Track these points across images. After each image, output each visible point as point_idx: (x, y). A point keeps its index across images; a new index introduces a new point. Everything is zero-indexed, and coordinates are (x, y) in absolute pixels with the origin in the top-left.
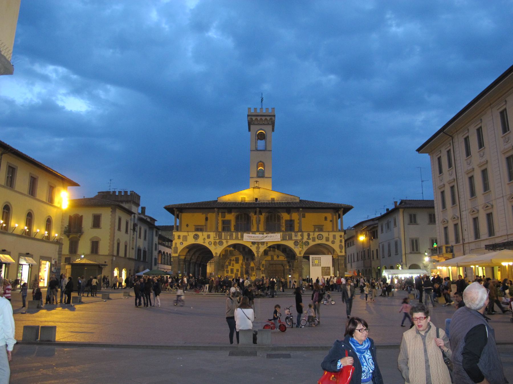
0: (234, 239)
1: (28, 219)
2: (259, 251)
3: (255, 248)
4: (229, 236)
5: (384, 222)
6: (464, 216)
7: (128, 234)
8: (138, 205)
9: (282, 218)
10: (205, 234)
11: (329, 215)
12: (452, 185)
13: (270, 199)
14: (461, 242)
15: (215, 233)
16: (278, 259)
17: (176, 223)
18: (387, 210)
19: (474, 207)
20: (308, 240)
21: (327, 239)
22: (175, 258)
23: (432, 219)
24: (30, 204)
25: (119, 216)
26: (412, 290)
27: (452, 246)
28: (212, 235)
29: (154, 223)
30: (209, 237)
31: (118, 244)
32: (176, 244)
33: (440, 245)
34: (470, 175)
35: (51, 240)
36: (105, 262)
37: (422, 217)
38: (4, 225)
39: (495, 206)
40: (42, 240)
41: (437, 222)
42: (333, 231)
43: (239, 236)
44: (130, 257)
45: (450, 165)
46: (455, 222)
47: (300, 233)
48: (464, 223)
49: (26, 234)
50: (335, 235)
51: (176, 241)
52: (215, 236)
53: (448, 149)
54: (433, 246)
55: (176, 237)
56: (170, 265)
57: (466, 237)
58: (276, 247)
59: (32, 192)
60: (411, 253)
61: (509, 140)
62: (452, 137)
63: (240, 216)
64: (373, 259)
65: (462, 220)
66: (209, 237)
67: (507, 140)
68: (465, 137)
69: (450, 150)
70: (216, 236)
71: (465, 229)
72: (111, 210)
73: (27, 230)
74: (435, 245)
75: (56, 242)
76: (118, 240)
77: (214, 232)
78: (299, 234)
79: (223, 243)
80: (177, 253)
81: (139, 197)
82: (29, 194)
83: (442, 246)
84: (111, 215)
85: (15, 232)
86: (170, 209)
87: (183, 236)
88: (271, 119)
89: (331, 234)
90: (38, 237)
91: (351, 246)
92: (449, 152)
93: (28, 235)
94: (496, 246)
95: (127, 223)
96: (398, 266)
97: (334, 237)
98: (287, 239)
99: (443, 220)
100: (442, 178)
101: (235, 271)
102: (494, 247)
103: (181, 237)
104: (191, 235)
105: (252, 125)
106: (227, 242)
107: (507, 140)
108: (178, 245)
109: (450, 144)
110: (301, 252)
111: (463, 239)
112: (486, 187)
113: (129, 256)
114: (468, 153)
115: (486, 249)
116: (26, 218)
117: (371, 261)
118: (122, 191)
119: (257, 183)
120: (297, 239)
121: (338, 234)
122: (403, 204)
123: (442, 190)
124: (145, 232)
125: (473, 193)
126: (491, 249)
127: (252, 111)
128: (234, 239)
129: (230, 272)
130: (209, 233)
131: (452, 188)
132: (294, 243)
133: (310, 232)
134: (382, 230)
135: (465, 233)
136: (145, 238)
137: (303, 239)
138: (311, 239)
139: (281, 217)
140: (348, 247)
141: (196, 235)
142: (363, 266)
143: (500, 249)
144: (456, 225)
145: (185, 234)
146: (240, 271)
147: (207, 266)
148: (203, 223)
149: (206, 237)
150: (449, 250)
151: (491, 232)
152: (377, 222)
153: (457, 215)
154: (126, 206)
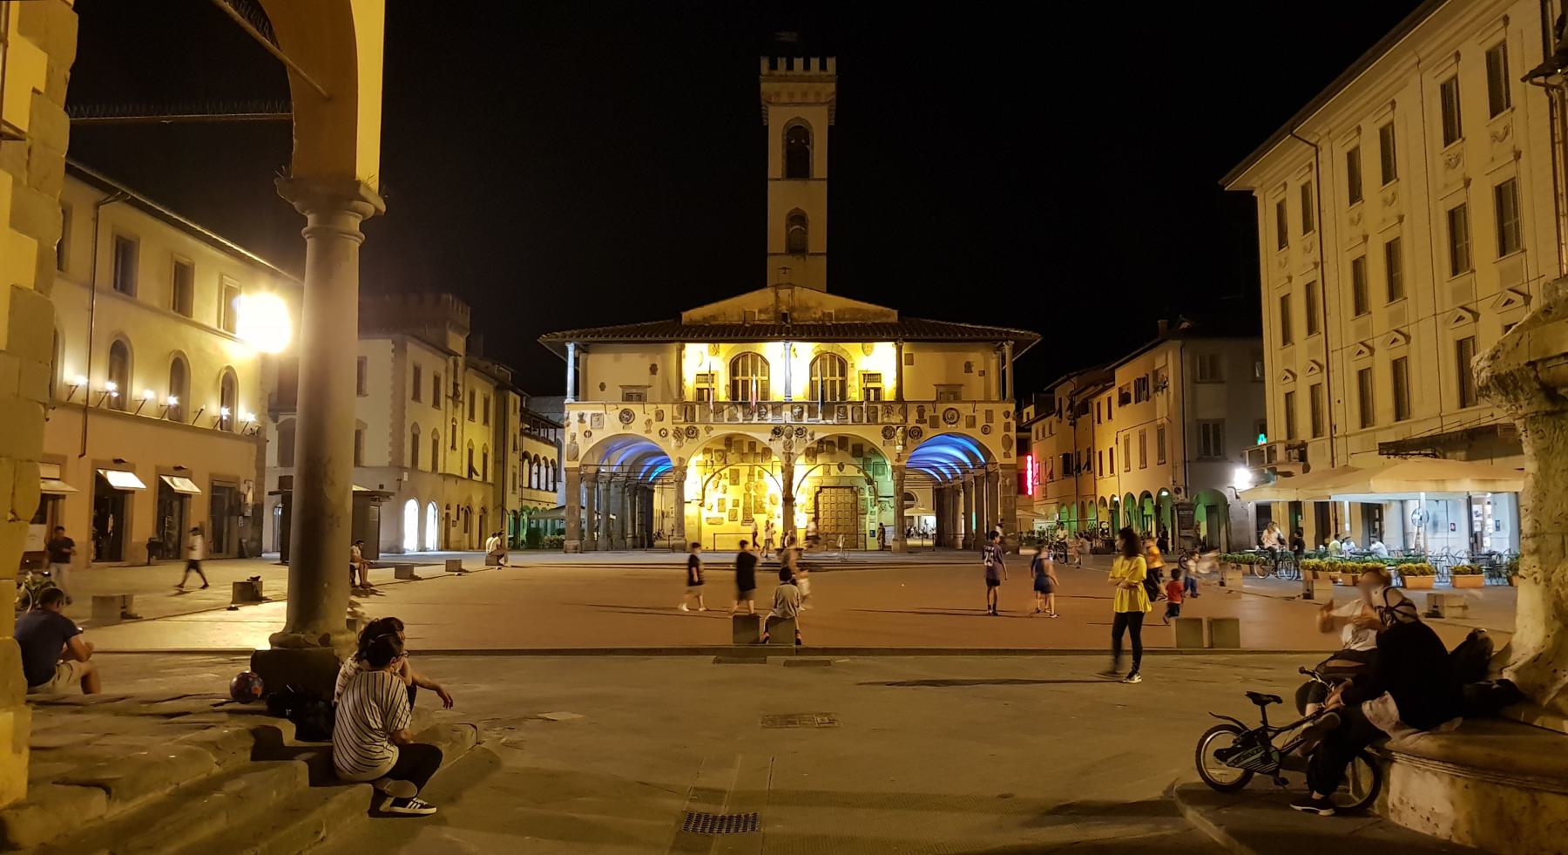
4: (712, 415)
6: (1335, 365)
7: (439, 409)
10: (651, 409)
15: (675, 406)
16: (841, 474)
20: (919, 425)
21: (972, 423)
22: (570, 473)
24: (114, 314)
26: (1022, 545)
30: (660, 416)
31: (471, 452)
32: (573, 437)
36: (381, 487)
42: (988, 400)
43: (740, 415)
50: (991, 411)
51: (573, 428)
53: (1302, 182)
57: (1338, 420)
58: (836, 441)
59: (181, 303)
62: (1316, 146)
63: (740, 361)
66: (660, 416)
69: (1310, 182)
71: (1337, 400)
77: (673, 403)
80: (578, 460)
87: (593, 415)
89: (982, 408)
90: (149, 412)
93: (175, 419)
95: (437, 380)
97: (989, 415)
102: (1397, 449)
103: (587, 419)
108: (580, 439)
109: (1310, 165)
113: (444, 468)
114: (1355, 195)
115: (1380, 454)
125: (1360, 306)
129: (715, 508)
130: (661, 407)
135: (1338, 411)
136: (486, 421)
138: (928, 421)
139: (849, 362)
142: (447, 472)
146: (741, 504)
147: (653, 491)
149: (653, 417)
150: (1295, 453)
151: (1401, 410)
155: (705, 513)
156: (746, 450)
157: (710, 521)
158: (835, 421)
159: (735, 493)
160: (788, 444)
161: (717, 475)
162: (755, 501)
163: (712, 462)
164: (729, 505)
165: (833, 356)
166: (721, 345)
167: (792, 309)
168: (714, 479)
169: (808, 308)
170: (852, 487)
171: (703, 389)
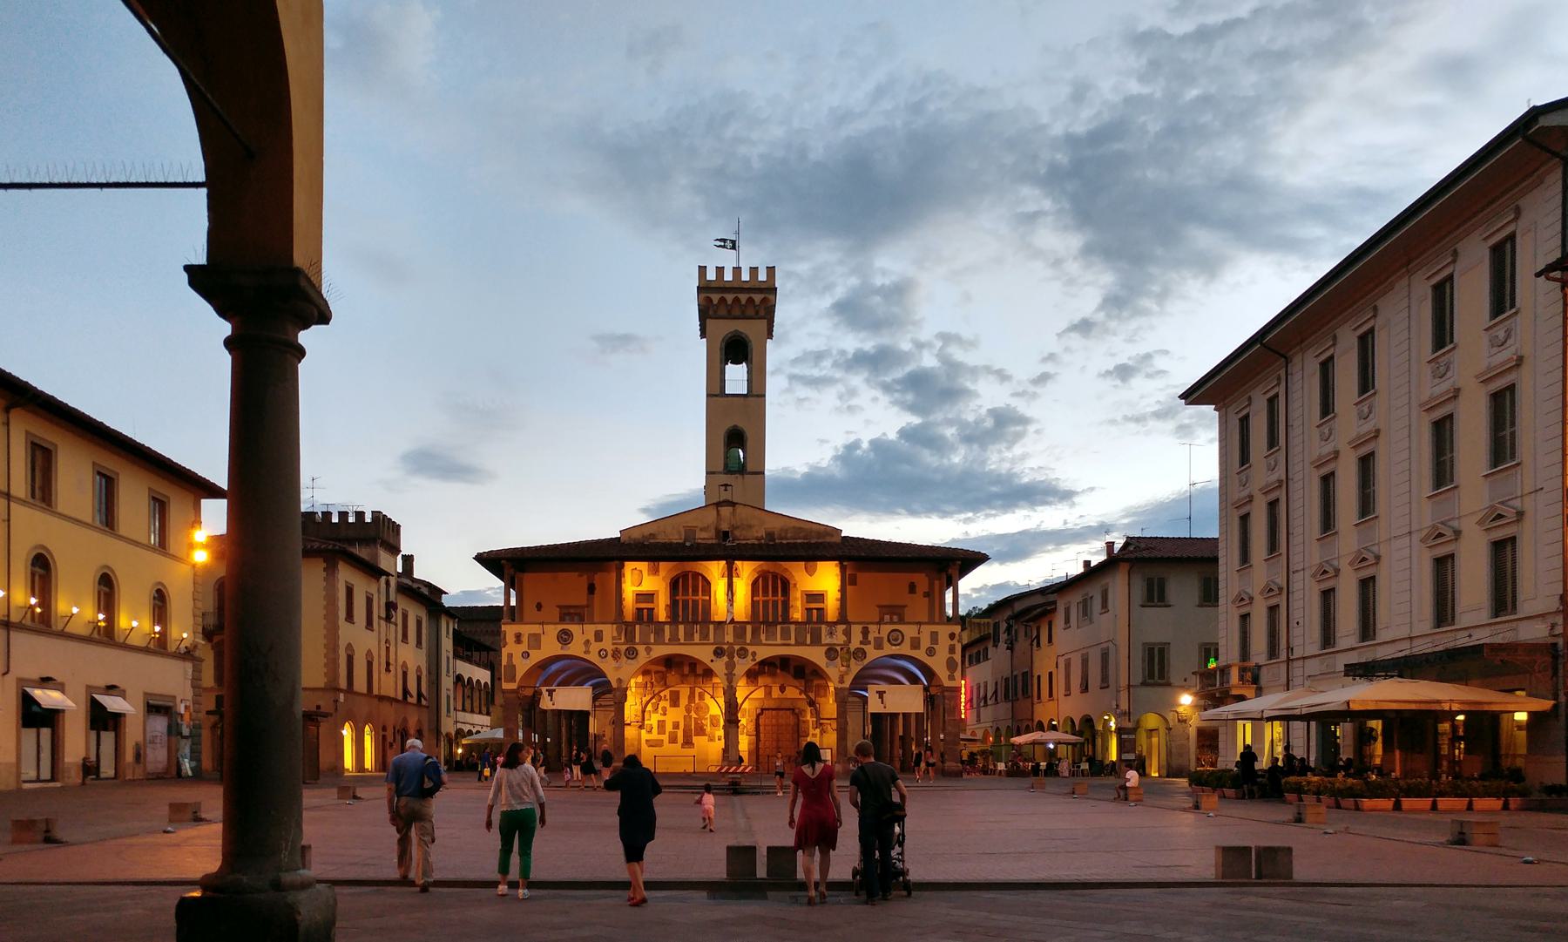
0: (667, 641)
1: (102, 593)
2: (735, 675)
3: (724, 667)
4: (652, 636)
5: (1075, 598)
8: (394, 549)
9: (795, 585)
10: (590, 629)
11: (921, 580)
12: (1272, 497)
13: (762, 533)
14: (1283, 657)
15: (615, 626)
16: (783, 696)
17: (507, 600)
18: (1087, 563)
19: (1327, 562)
20: (862, 646)
21: (915, 644)
22: (507, 695)
23: (1209, 596)
25: (346, 582)
27: (1259, 667)
28: (609, 630)
29: (440, 598)
30: (599, 636)
31: (405, 674)
32: (510, 656)
33: (1225, 664)
34: (1325, 470)
35: (172, 648)
36: (318, 707)
37: (1183, 589)
38: (38, 610)
39: (1384, 562)
40: (145, 650)
41: (1222, 601)
42: (931, 622)
44: (383, 693)
45: (1272, 441)
46: (1273, 602)
47: (843, 627)
48: (1296, 604)
49: (37, 620)
52: (615, 634)
54: (1206, 666)
55: (510, 638)
56: (488, 714)
58: (778, 663)
60: (1144, 684)
61: (1448, 369)
64: (1039, 698)
65: (1290, 595)
66: (599, 636)
67: (1442, 369)
68: (1323, 357)
69: (1277, 396)
70: (619, 634)
72: (325, 565)
73: (102, 624)
74: (1212, 664)
75: (185, 653)
76: (349, 646)
78: (841, 628)
79: (637, 654)
81: (396, 528)
82: (33, 496)
83: (1229, 666)
84: (325, 579)
85: (70, 629)
86: (492, 561)
88: (764, 300)
89: (927, 630)
91: (978, 662)
92: (1272, 402)
94: (1373, 667)
95: (369, 601)
96: (1106, 717)
97: (934, 637)
98: (808, 642)
99: (1240, 594)
100: (1247, 477)
101: (669, 728)
103: (525, 639)
104: (553, 630)
105: (711, 318)
106: (648, 650)
107: (1442, 369)
109: (1279, 379)
110: (845, 677)
111: (1288, 648)
112: (1366, 505)
113: (379, 689)
114: (1327, 408)
116: (29, 572)
117: (1033, 704)
118: (351, 510)
119: (726, 490)
120: (835, 642)
121: (944, 631)
122: (1131, 548)
123: (1243, 511)
124: (419, 623)
126: (1361, 676)
127: (711, 275)
128: (667, 641)
129: (655, 730)
130: (600, 627)
131: (1273, 505)
132: (826, 653)
133: (868, 623)
134: (1067, 621)
135: (1296, 632)
136: (419, 643)
137: (850, 642)
139: (792, 582)
140: (970, 664)
141: (564, 632)
143: (1387, 675)
144: (1273, 609)
145: (536, 629)
148: (580, 598)
149: (592, 639)
150: (1249, 676)
151: (1367, 628)
152: (1052, 598)
153: (1278, 581)
154: (362, 552)
155: (644, 735)
156: (686, 670)
157: (651, 743)
158: (779, 641)
159: (675, 715)
160: (730, 666)
161: (657, 697)
162: (696, 723)
163: (652, 683)
164: (669, 728)
165: (775, 576)
166: (661, 563)
167: (734, 527)
168: (654, 701)
169: (750, 527)
170: (793, 710)
171: (643, 609)
